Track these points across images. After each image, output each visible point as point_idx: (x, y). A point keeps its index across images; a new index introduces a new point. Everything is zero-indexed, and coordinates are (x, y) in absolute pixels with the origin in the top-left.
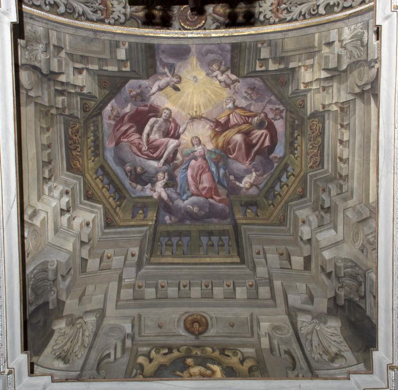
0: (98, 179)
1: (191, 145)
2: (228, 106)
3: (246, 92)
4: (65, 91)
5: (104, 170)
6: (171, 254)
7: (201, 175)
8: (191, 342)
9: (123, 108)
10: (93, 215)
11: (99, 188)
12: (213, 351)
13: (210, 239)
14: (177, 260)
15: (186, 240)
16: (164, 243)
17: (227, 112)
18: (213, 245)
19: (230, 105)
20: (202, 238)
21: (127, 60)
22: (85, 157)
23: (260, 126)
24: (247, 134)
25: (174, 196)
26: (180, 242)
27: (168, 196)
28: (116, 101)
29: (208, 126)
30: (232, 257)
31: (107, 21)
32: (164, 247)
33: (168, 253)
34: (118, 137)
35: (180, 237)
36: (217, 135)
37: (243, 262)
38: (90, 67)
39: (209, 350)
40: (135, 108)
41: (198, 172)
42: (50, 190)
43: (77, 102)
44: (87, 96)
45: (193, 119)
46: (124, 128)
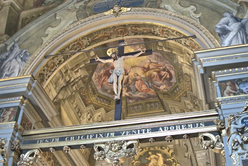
0: (98, 101)
1: (134, 77)
2: (148, 62)
3: (155, 57)
4: (75, 83)
5: (100, 97)
6: (135, 112)
7: (141, 86)
8: (150, 145)
9: (100, 73)
10: (101, 112)
11: (100, 103)
12: (158, 148)
13: (151, 105)
14: (139, 114)
15: (140, 106)
16: (131, 109)
17: (148, 64)
18: (152, 107)
19: (149, 61)
20: (147, 105)
21: (95, 55)
22: (91, 97)
23: (164, 70)
24: (159, 72)
25: (132, 94)
26: (138, 108)
27: (129, 94)
28: (96, 72)
29: (140, 69)
30: (161, 110)
31: (82, 49)
32: (132, 110)
33: (135, 112)
34: (101, 83)
35: (138, 106)
36: (145, 72)
37: (166, 111)
38: (81, 67)
39: (157, 148)
40: (105, 70)
41: (140, 84)
42: (83, 118)
43: (81, 83)
44: (84, 77)
45: (132, 67)
46: (103, 79)
